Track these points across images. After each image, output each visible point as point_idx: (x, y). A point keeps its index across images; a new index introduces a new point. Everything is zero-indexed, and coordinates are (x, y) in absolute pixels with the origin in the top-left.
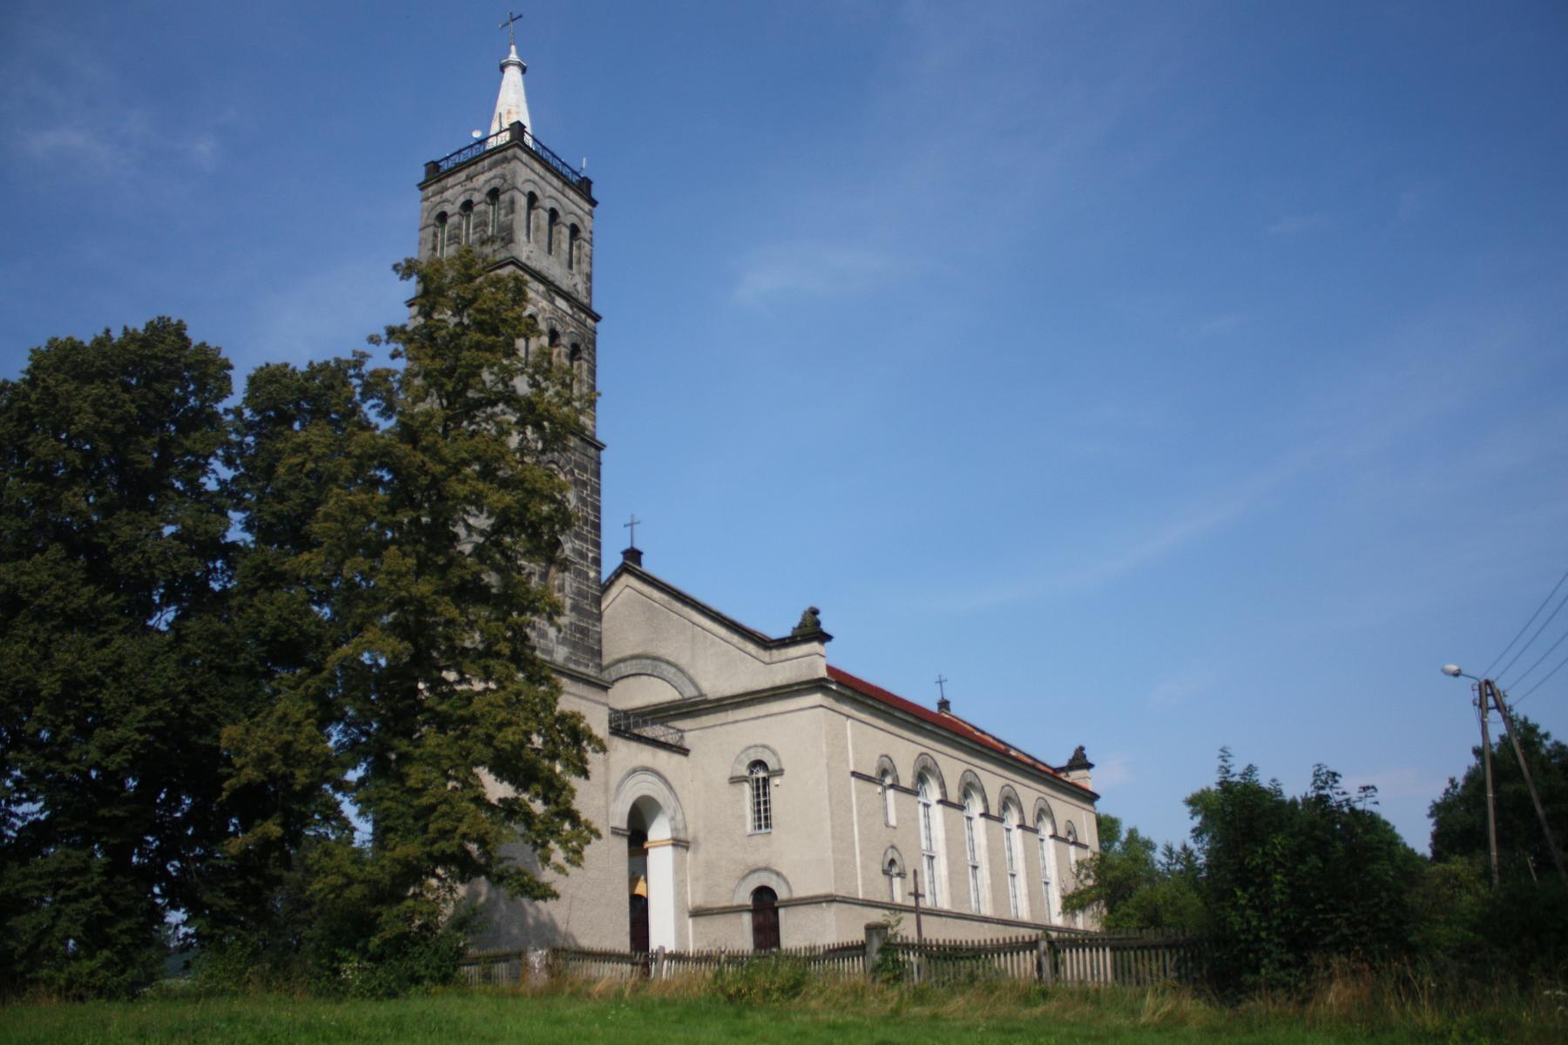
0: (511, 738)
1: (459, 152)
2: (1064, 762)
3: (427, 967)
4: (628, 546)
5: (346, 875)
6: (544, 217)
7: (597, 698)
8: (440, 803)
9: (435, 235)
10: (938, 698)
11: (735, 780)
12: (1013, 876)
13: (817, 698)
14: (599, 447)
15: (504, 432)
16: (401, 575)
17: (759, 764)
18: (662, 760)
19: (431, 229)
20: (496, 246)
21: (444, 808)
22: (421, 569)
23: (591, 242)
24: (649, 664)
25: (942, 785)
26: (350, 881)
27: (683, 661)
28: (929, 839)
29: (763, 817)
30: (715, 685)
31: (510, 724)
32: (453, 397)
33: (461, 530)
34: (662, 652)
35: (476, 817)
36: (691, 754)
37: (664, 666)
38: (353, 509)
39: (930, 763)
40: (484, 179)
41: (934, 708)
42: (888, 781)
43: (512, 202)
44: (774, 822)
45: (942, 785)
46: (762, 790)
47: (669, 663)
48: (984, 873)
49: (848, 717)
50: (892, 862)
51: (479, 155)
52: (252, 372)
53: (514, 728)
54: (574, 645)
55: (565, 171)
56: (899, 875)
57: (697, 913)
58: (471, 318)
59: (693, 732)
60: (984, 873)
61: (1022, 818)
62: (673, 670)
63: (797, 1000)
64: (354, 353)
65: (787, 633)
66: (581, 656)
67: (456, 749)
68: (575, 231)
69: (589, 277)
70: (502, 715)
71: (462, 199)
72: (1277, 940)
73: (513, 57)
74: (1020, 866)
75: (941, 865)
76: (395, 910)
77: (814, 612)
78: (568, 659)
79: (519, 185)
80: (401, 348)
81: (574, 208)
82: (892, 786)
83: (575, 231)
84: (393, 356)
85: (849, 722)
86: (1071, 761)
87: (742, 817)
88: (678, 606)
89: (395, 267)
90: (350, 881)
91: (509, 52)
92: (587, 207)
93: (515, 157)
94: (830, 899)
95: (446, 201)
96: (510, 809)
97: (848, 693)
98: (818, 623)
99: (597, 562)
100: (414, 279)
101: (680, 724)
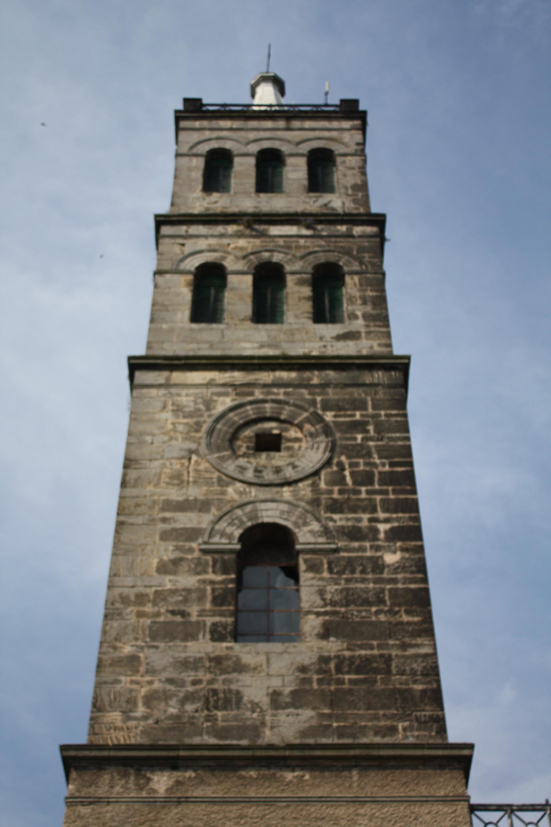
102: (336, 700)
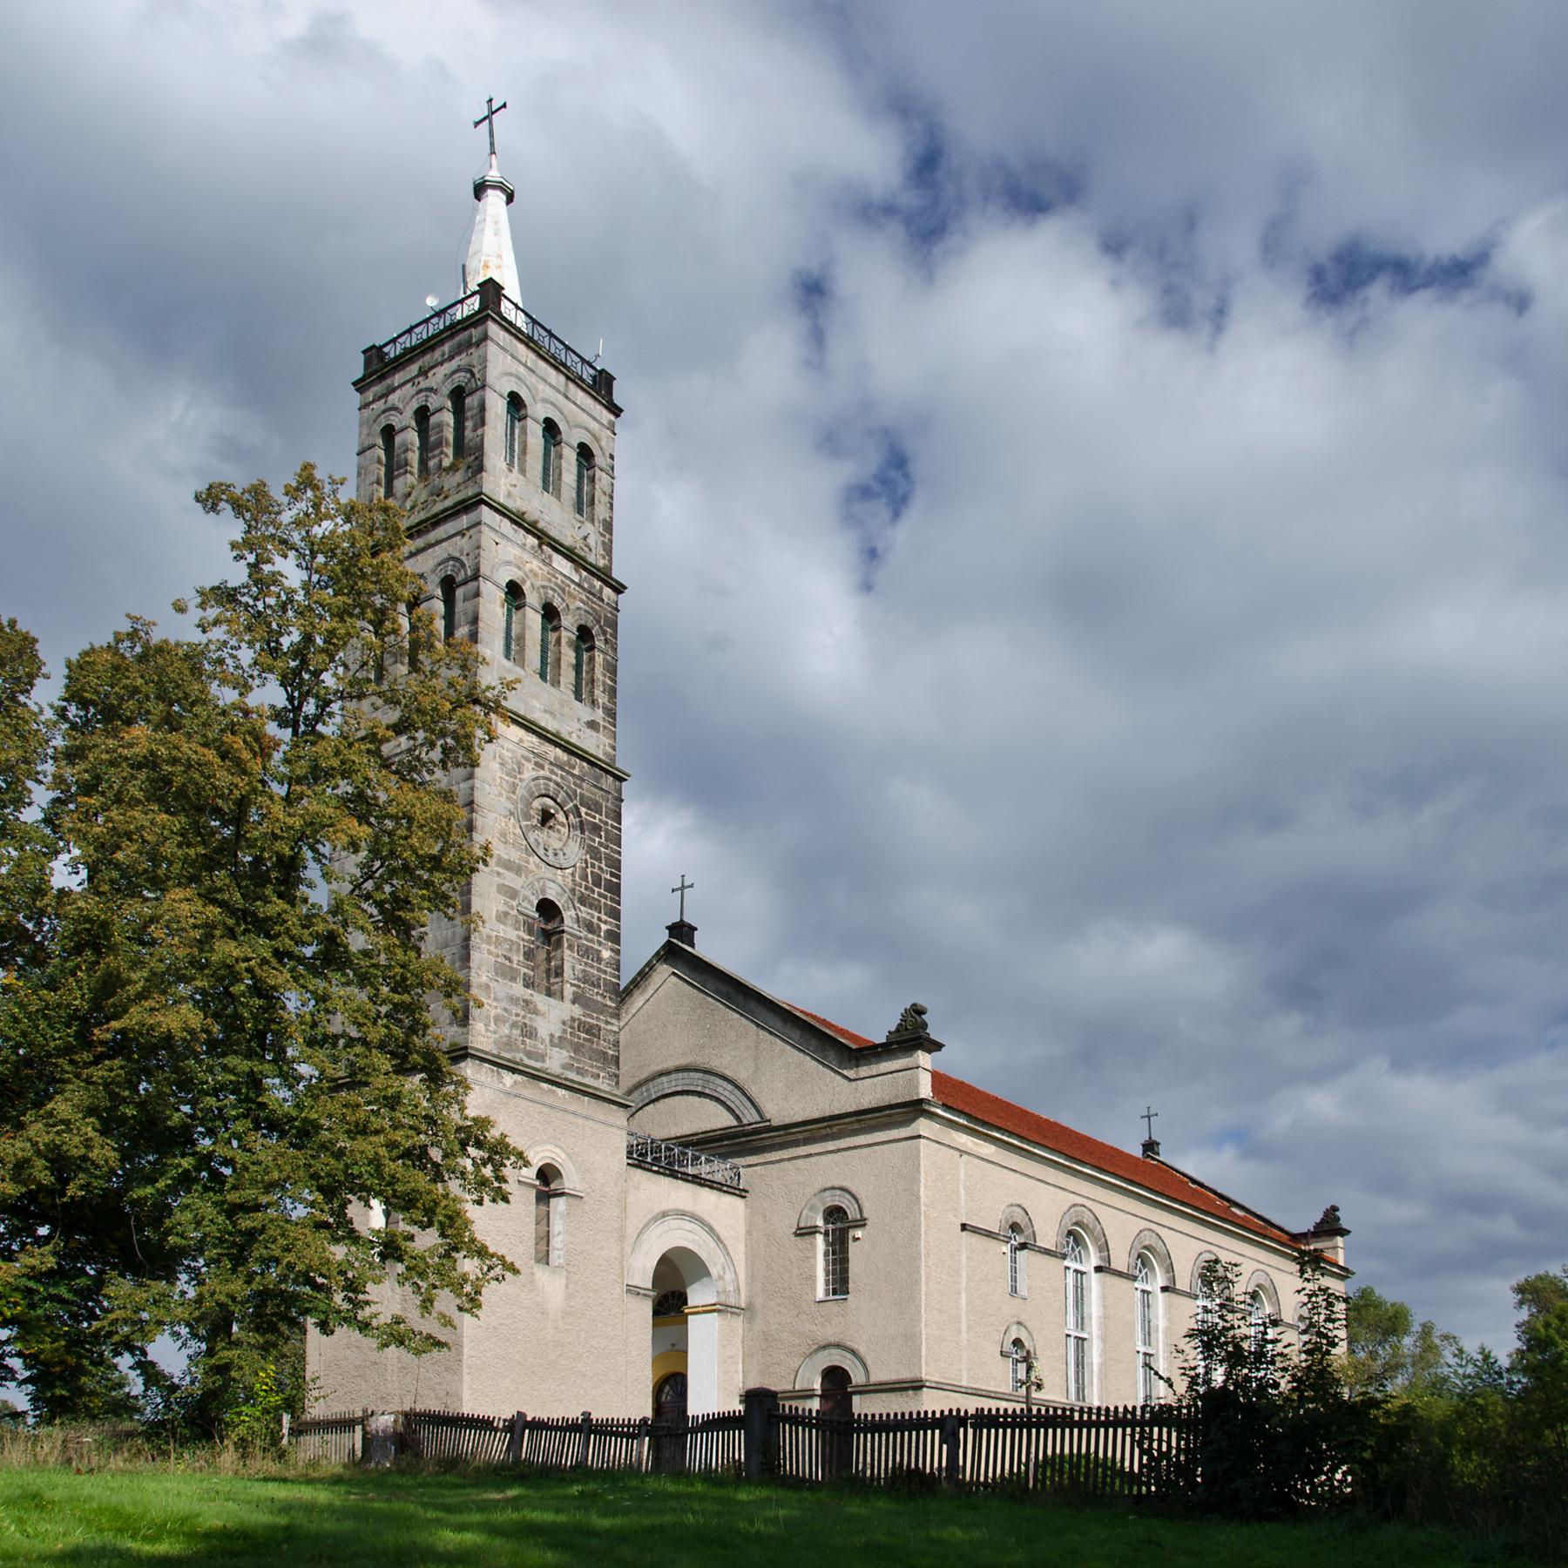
1: (410, 331)
18: (707, 1201)
27: (741, 1076)
29: (840, 1282)
30: (782, 1107)
39: (1087, 1218)
65: (880, 1038)
66: (586, 1063)
68: (585, 453)
69: (608, 526)
71: (415, 405)
77: (918, 1011)
83: (585, 453)
86: (1317, 1226)
92: (606, 416)
102: (577, 1048)
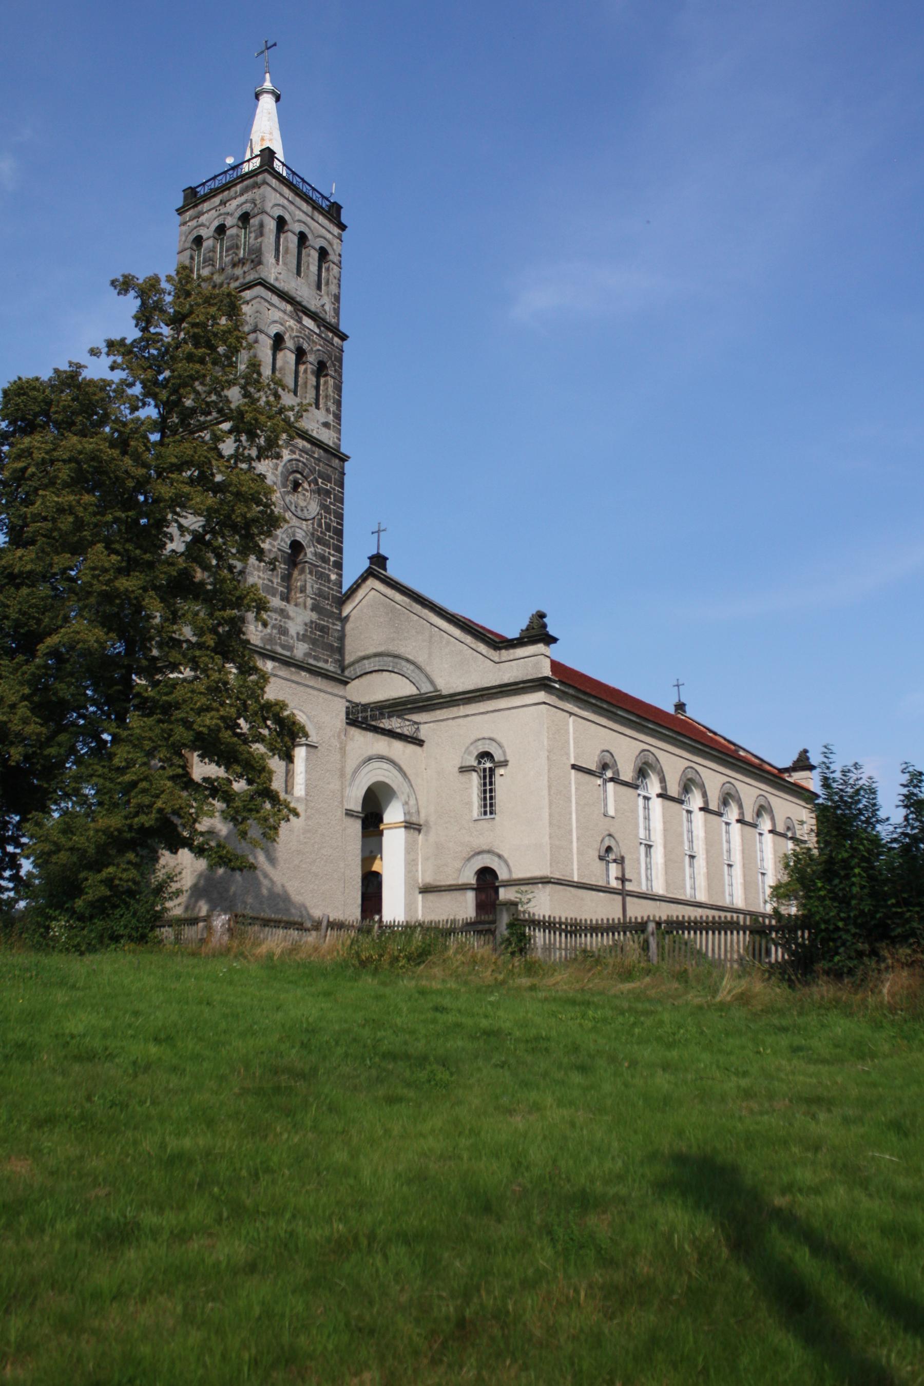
0: (208, 722)
1: (314, 189)
2: (788, 764)
3: (126, 927)
4: (374, 552)
5: (55, 843)
6: (293, 240)
7: (336, 691)
8: (142, 780)
9: (192, 258)
10: (675, 701)
11: (464, 770)
12: (730, 866)
13: (541, 696)
14: (343, 459)
15: (217, 439)
16: (105, 571)
17: (486, 755)
18: (397, 749)
19: (188, 253)
20: (246, 269)
21: (144, 785)
22: (129, 567)
23: (339, 265)
24: (390, 661)
25: (663, 780)
26: (58, 848)
27: (421, 659)
28: (648, 829)
29: (488, 805)
30: (449, 681)
31: (208, 709)
32: (169, 406)
33: (173, 529)
34: (402, 651)
35: (171, 793)
36: (425, 744)
37: (404, 663)
38: (61, 510)
39: (651, 759)
40: (236, 205)
41: (671, 710)
42: (609, 774)
43: (261, 225)
44: (497, 808)
45: (663, 780)
46: (488, 778)
47: (408, 660)
48: (701, 862)
49: (571, 714)
50: (609, 849)
51: (235, 180)
52: (6, 386)
53: (213, 713)
54: (314, 642)
55: (315, 196)
56: (615, 861)
57: (426, 890)
58: (189, 333)
59: (428, 724)
60: (701, 862)
61: (742, 813)
62: (412, 667)
63: (422, 967)
64: (71, 364)
66: (323, 654)
67: (158, 731)
68: (323, 254)
69: (337, 298)
70: (203, 701)
71: (216, 224)
72: (853, 930)
73: (268, 85)
74: (737, 858)
75: (658, 854)
76: (99, 877)
78: (307, 655)
79: (268, 210)
80: (119, 359)
81: (324, 232)
82: (612, 780)
83: (323, 254)
84: (112, 368)
85: (573, 717)
86: (795, 763)
87: (470, 803)
88: (417, 608)
89: (113, 283)
90: (58, 848)
91: (264, 80)
92: (336, 231)
93: (264, 182)
94: (546, 881)
95: (202, 225)
96: (214, 788)
97: (571, 691)
98: (544, 626)
99: (339, 565)
100: (132, 293)
101: (416, 717)
